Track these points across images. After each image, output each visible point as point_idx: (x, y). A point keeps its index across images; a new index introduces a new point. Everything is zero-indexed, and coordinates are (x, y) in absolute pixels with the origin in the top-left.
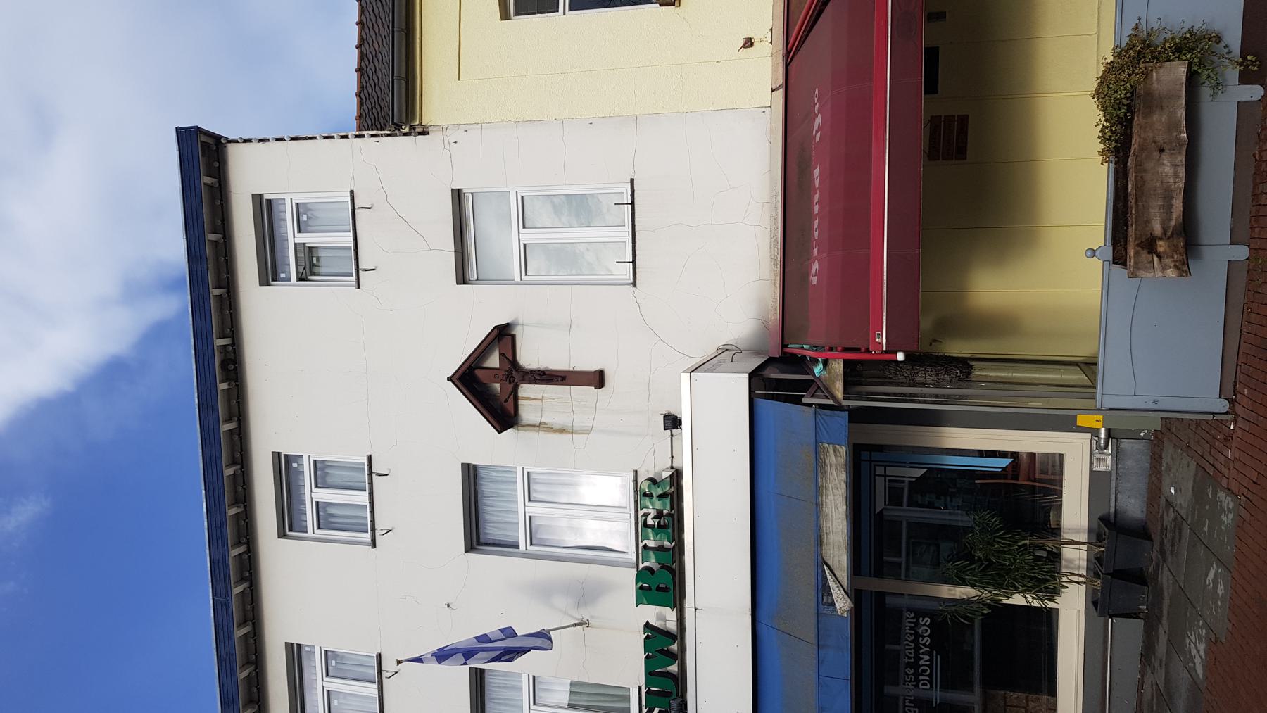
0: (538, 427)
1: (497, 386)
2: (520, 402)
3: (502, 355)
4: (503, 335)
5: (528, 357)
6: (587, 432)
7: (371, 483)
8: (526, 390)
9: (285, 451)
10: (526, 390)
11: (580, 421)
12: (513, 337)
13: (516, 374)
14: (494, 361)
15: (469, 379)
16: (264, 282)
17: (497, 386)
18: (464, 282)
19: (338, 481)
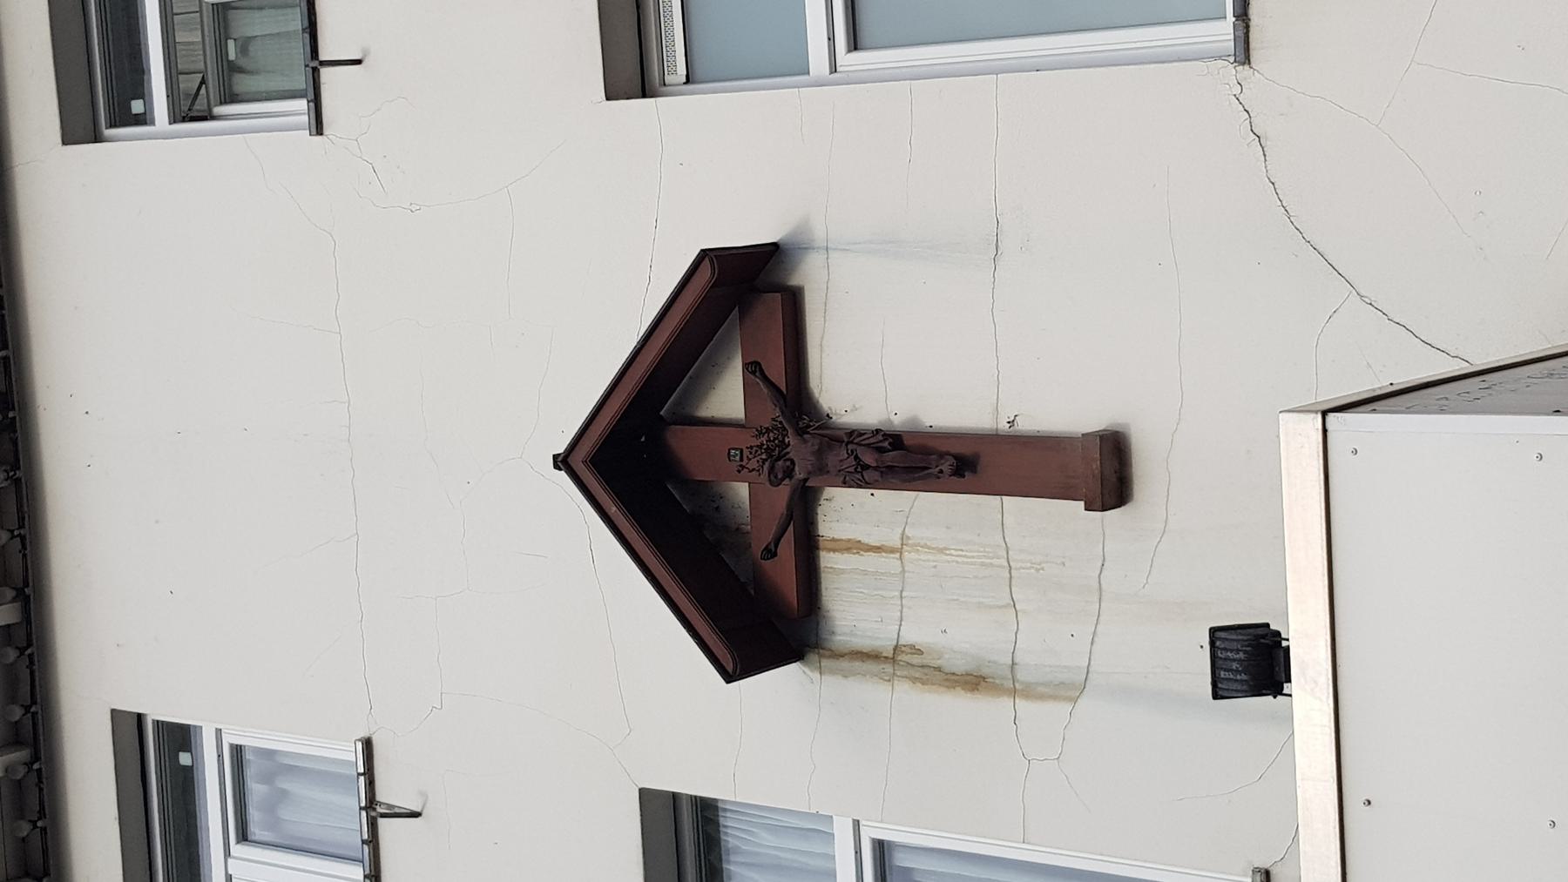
0: (892, 661)
1: (742, 490)
2: (827, 560)
3: (753, 369)
4: (743, 295)
5: (863, 372)
6: (1067, 690)
7: (373, 841)
8: (847, 512)
9: (159, 710)
10: (847, 512)
11: (1042, 643)
12: (794, 301)
13: (814, 449)
14: (727, 397)
15: (635, 461)
16: (80, 127)
17: (742, 490)
18: (645, 90)
19: (256, 838)
